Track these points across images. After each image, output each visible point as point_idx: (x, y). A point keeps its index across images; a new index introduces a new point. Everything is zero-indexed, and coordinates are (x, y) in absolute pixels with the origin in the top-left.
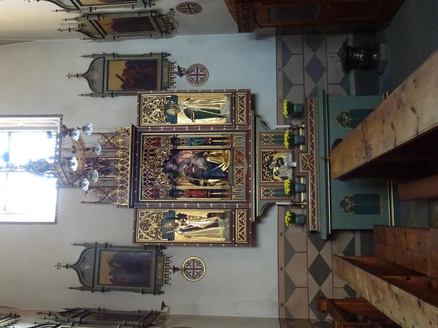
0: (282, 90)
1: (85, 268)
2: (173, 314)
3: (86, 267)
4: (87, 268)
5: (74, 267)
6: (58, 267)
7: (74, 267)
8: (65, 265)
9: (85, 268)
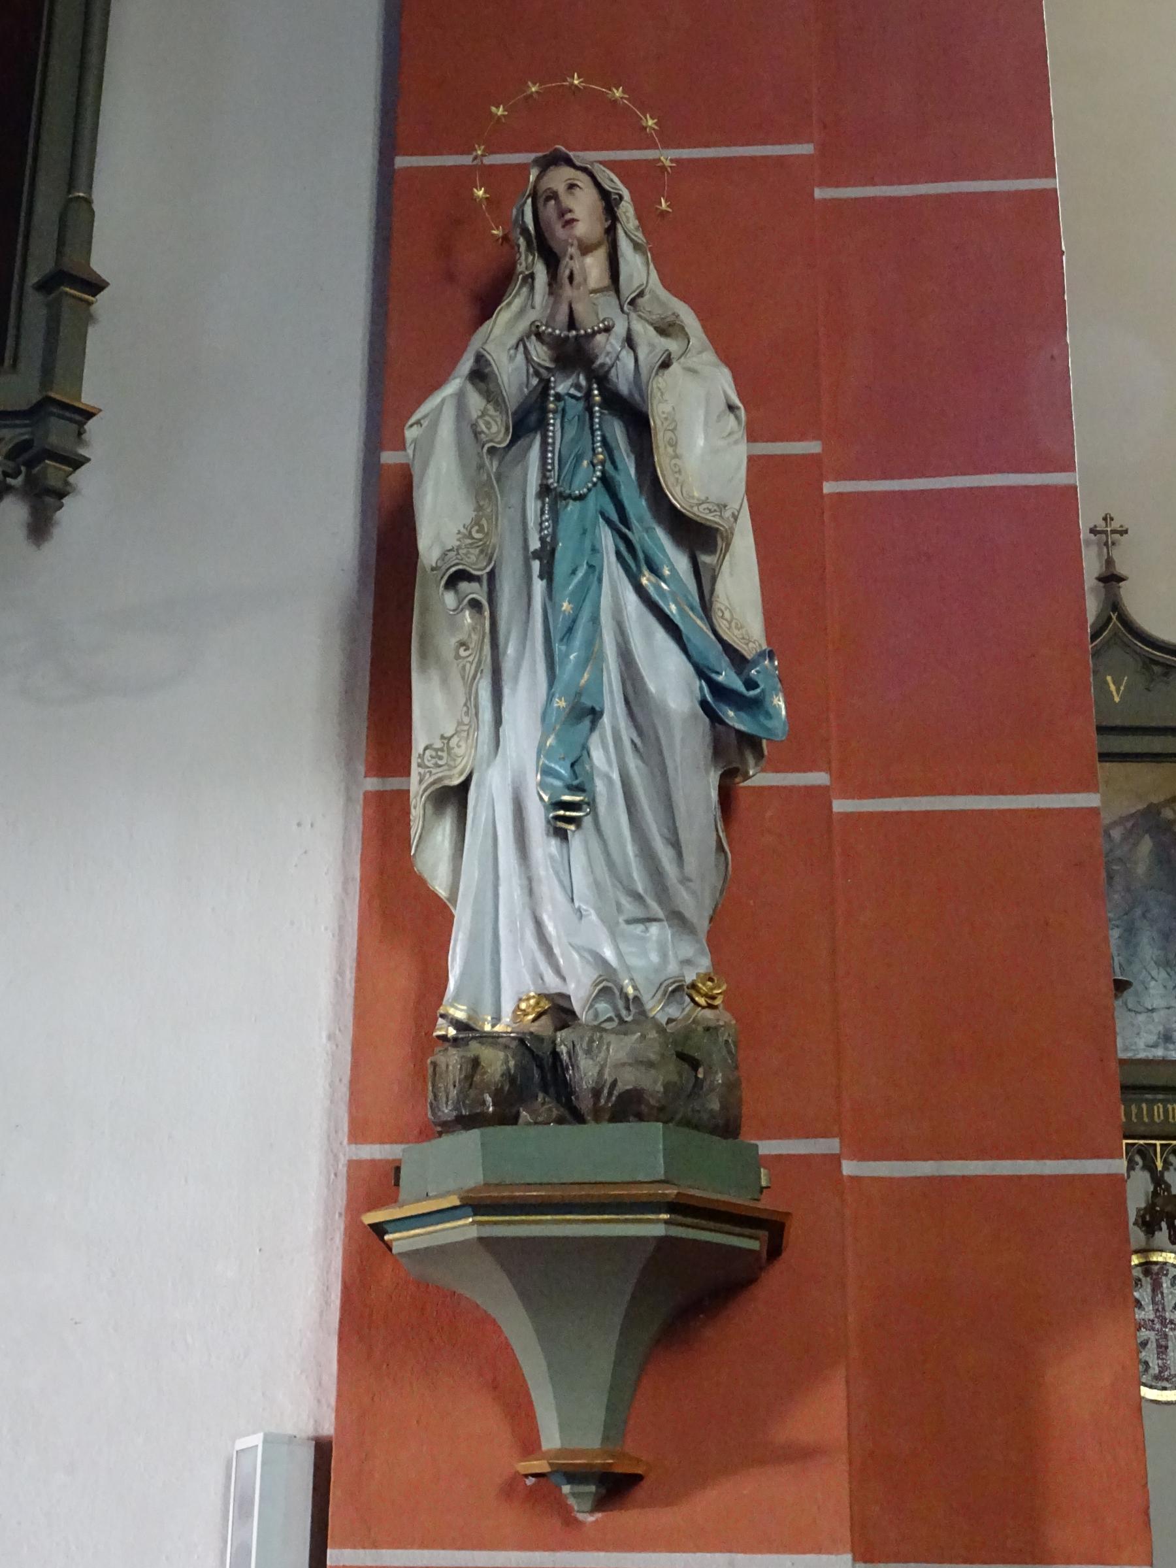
0: (539, 1348)
1: (1109, 678)
2: (767, 1152)
3: (1117, 684)
4: (1113, 688)
5: (1110, 619)
6: (1105, 532)
7: (1114, 617)
8: (1121, 569)
9: (1109, 678)
